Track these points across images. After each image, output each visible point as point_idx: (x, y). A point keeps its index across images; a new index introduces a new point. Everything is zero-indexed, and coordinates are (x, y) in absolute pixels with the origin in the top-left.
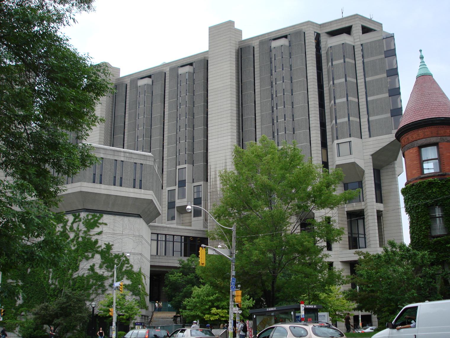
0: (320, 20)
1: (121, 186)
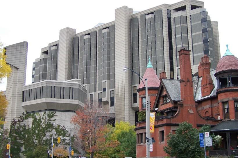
0: (170, 3)
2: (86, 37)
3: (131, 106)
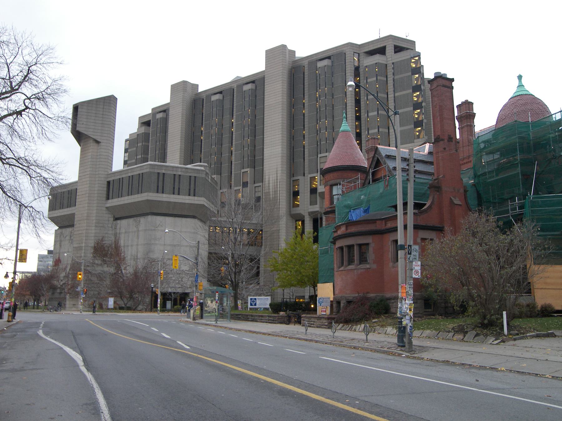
1: (179, 194)
2: (214, 98)
3: (290, 212)
